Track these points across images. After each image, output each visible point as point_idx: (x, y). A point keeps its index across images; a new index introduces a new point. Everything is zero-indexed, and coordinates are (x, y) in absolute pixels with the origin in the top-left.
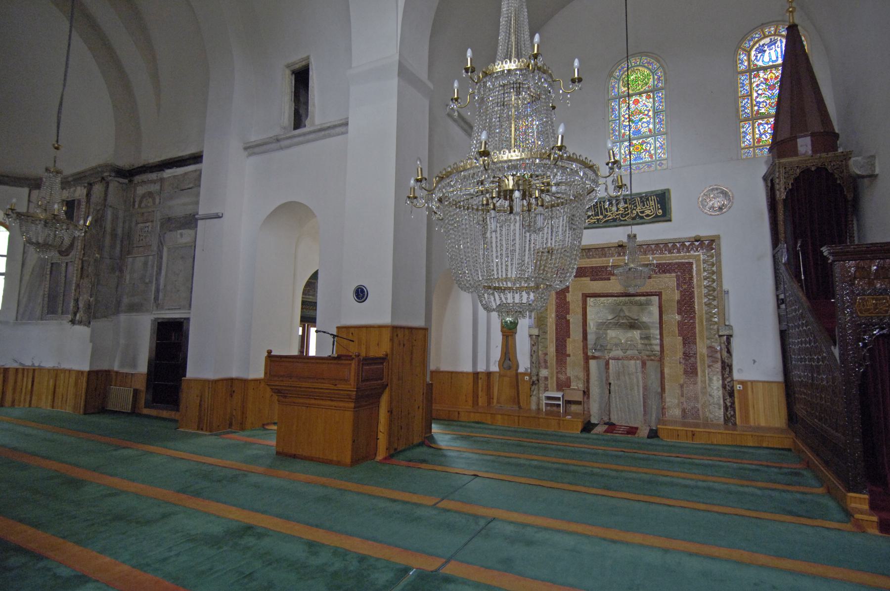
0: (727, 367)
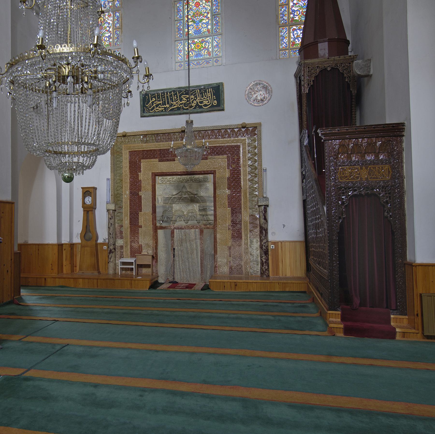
0: (264, 231)
